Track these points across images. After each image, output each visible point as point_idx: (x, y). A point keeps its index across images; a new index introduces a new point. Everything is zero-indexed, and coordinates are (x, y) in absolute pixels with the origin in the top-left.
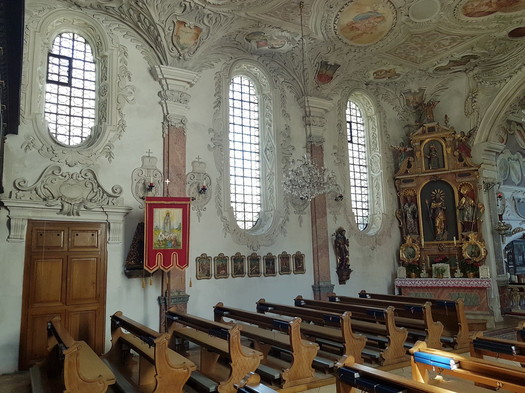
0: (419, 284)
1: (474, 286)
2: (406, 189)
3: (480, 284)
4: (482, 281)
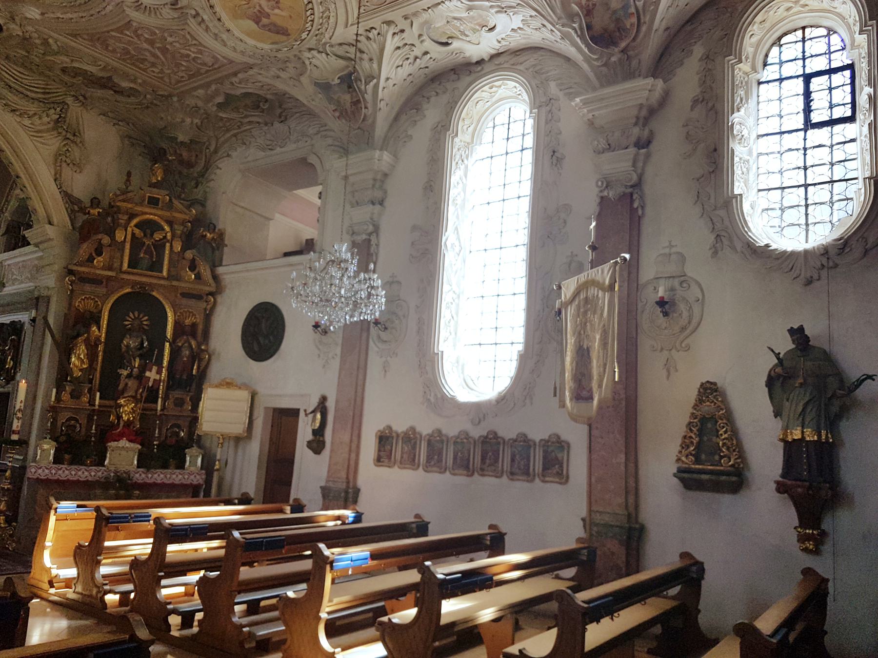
1: (42, 477)
4: (190, 474)
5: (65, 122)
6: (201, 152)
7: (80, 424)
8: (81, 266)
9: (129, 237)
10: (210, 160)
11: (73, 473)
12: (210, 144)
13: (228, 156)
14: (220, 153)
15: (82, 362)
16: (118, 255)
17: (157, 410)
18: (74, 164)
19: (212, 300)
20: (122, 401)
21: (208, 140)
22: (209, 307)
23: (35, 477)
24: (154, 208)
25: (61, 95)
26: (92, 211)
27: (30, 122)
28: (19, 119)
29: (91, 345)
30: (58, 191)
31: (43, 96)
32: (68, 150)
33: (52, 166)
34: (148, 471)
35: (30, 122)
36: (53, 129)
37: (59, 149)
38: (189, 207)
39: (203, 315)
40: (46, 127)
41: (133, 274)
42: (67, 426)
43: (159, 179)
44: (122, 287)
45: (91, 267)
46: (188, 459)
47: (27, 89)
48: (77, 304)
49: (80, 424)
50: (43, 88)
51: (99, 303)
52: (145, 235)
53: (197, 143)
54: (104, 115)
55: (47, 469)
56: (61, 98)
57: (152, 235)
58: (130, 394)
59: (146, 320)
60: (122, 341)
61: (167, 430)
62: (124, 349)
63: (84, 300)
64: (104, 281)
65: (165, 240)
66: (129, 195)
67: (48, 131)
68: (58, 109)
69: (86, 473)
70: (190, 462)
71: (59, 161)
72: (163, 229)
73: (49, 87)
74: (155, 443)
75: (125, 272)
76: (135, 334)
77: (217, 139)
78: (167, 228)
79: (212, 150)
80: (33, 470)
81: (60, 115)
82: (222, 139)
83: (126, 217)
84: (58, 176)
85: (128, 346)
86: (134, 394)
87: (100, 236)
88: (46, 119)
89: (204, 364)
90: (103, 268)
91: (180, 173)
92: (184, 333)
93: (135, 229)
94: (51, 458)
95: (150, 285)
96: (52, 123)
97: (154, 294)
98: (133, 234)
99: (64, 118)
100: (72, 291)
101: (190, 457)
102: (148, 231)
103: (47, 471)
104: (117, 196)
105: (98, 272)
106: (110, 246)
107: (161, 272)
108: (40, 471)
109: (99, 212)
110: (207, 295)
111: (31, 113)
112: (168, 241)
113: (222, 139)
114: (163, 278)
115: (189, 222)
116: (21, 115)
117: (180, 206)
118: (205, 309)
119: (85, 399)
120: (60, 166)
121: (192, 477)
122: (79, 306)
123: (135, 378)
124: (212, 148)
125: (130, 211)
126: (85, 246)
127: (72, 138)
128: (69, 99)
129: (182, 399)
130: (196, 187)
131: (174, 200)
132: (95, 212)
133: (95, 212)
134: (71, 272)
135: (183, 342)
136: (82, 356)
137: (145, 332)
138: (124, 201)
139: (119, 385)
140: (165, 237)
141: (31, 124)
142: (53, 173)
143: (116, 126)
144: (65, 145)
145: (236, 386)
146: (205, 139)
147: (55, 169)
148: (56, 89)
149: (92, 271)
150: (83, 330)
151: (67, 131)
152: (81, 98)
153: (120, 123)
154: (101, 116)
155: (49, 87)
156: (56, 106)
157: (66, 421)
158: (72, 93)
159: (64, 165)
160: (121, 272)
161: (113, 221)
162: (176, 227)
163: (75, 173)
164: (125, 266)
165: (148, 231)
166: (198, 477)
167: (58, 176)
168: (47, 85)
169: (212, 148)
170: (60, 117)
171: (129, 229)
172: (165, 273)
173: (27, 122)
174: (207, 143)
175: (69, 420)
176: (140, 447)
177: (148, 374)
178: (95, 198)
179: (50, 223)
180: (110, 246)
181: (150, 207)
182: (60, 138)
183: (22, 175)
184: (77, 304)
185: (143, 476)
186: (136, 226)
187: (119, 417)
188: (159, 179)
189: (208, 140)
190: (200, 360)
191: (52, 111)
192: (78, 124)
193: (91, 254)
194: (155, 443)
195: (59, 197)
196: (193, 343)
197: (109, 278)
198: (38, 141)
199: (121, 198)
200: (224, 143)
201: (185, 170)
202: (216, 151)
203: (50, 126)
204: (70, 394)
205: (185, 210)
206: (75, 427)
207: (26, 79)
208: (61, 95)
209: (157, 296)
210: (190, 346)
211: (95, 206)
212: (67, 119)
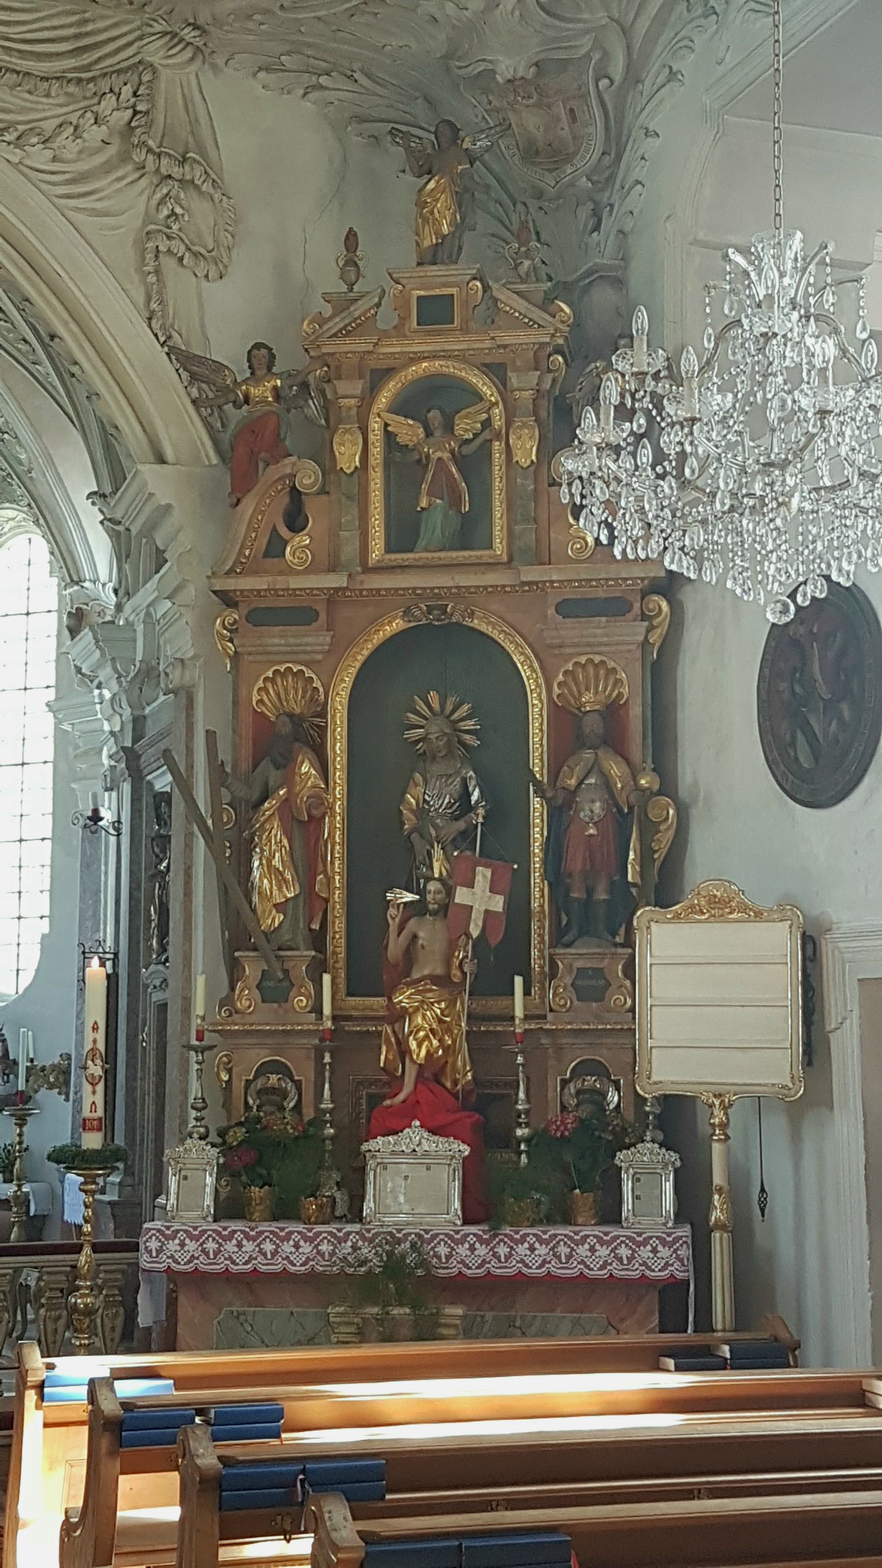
0: (535, 1261)
2: (583, 660)
3: (216, 1254)
5: (150, 125)
6: (584, 97)
7: (298, 1085)
8: (254, 573)
9: (377, 452)
10: (620, 122)
11: (268, 1247)
12: (606, 56)
13: (672, 75)
14: (648, 83)
15: (282, 881)
16: (350, 516)
17: (513, 1018)
18: (196, 255)
19: (664, 605)
20: (403, 998)
21: (597, 44)
22: (655, 637)
23: (162, 1266)
24: (439, 333)
25: (129, 44)
26: (254, 391)
27: (49, 154)
28: (15, 155)
29: (301, 822)
30: (161, 353)
31: (72, 62)
32: (173, 213)
33: (136, 277)
34: (495, 1228)
35: (49, 154)
36: (124, 158)
37: (148, 219)
38: (546, 303)
39: (638, 665)
40: (98, 160)
41: (403, 568)
42: (259, 1092)
43: (445, 229)
44: (375, 621)
45: (281, 573)
46: (627, 1187)
47: (39, 56)
48: (255, 698)
49: (298, 1085)
50: (77, 36)
51: (317, 684)
52: (429, 434)
53: (563, 64)
54: (267, 69)
55: (192, 1238)
56: (130, 51)
57: (449, 427)
58: (426, 972)
59: (468, 717)
60: (402, 799)
61: (565, 1083)
62: (410, 821)
63: (272, 680)
64: (321, 608)
65: (486, 435)
66: (357, 309)
67: (106, 168)
68: (127, 91)
69: (306, 1248)
70: (636, 1198)
71: (150, 256)
72: (480, 398)
73: (89, 28)
74: (519, 1132)
75: (380, 569)
76: (436, 768)
77: (626, 32)
78: (488, 390)
79: (618, 78)
80: (153, 1245)
81: (134, 106)
82: (642, 26)
83: (357, 387)
84: (154, 306)
85: (422, 812)
86: (439, 971)
87: (286, 466)
88: (95, 134)
89: (664, 840)
90: (308, 571)
91: (539, 195)
92: (581, 742)
93: (390, 417)
94: (209, 1201)
95: (460, 593)
96: (116, 141)
97: (476, 623)
98: (389, 436)
99: (147, 113)
100: (236, 657)
101: (636, 1180)
102: (434, 416)
103: (191, 1245)
104: (321, 320)
105: (295, 583)
106: (323, 491)
107: (490, 547)
108: (173, 1246)
109: (275, 388)
110: (644, 594)
111: (49, 126)
112: (498, 436)
113: (642, 26)
114: (492, 566)
115: (558, 351)
116: (18, 142)
117: (520, 304)
118: (645, 644)
119: (301, 1001)
120: (157, 272)
121: (645, 1252)
122: (261, 702)
123: (434, 913)
124: (617, 69)
125: (373, 363)
126: (248, 505)
127: (176, 172)
128: (152, 47)
129: (599, 972)
130: (597, 228)
131: (499, 292)
132: (262, 391)
133: (262, 391)
134: (227, 599)
135: (579, 771)
136: (276, 862)
137: (470, 755)
138: (345, 332)
139: (386, 947)
140: (487, 424)
141: (54, 159)
142: (141, 300)
143: (314, 95)
144: (162, 202)
145: (744, 908)
146: (586, 43)
147: (146, 284)
148: (116, 25)
149: (281, 582)
150: (274, 776)
151: (159, 155)
152: (189, 34)
153: (323, 80)
154: (262, 75)
155: (89, 28)
156: (116, 81)
157: (256, 1077)
158: (158, 28)
159: (169, 264)
160: (367, 570)
161: (327, 408)
162: (514, 379)
163: (205, 284)
164: (377, 552)
165: (434, 416)
166: (664, 1252)
167: (154, 306)
168: (86, 21)
169: (617, 69)
170: (135, 113)
171: (375, 425)
172: (499, 547)
173: (40, 157)
174: (596, 56)
175: (265, 1069)
176: (466, 1150)
177: (462, 896)
178: (258, 346)
179: (161, 460)
180: (323, 491)
181: (429, 333)
182: (143, 182)
183: (61, 331)
184: (255, 698)
185: (482, 1250)
186: (400, 407)
187: (404, 1052)
188: (445, 229)
189: (597, 44)
190: (649, 829)
191: (110, 101)
192: (193, 123)
193: (274, 528)
194: (519, 1132)
195: (167, 368)
196: (616, 769)
197: (334, 597)
198: (77, 209)
199: (337, 324)
200: (652, 37)
201: (549, 178)
202: (633, 77)
203: (112, 150)
204: (258, 986)
205: (537, 314)
206: (284, 1094)
207: (18, 23)
208: (129, 44)
209: (484, 628)
210: (607, 783)
211: (260, 373)
212: (160, 118)
